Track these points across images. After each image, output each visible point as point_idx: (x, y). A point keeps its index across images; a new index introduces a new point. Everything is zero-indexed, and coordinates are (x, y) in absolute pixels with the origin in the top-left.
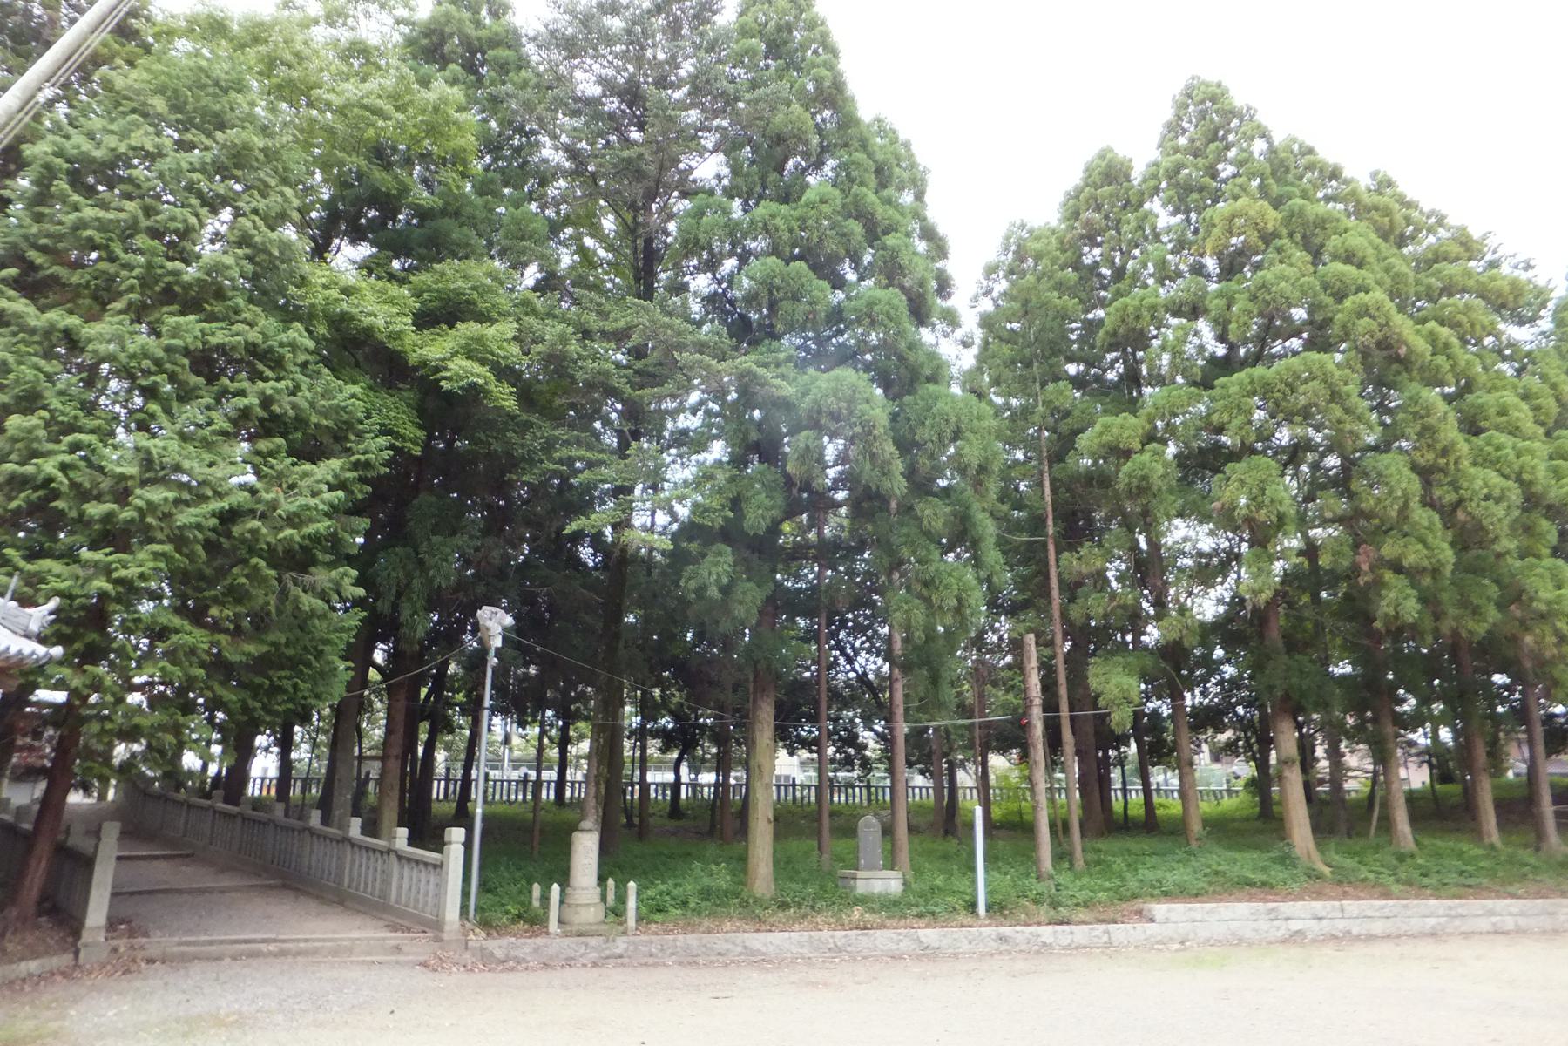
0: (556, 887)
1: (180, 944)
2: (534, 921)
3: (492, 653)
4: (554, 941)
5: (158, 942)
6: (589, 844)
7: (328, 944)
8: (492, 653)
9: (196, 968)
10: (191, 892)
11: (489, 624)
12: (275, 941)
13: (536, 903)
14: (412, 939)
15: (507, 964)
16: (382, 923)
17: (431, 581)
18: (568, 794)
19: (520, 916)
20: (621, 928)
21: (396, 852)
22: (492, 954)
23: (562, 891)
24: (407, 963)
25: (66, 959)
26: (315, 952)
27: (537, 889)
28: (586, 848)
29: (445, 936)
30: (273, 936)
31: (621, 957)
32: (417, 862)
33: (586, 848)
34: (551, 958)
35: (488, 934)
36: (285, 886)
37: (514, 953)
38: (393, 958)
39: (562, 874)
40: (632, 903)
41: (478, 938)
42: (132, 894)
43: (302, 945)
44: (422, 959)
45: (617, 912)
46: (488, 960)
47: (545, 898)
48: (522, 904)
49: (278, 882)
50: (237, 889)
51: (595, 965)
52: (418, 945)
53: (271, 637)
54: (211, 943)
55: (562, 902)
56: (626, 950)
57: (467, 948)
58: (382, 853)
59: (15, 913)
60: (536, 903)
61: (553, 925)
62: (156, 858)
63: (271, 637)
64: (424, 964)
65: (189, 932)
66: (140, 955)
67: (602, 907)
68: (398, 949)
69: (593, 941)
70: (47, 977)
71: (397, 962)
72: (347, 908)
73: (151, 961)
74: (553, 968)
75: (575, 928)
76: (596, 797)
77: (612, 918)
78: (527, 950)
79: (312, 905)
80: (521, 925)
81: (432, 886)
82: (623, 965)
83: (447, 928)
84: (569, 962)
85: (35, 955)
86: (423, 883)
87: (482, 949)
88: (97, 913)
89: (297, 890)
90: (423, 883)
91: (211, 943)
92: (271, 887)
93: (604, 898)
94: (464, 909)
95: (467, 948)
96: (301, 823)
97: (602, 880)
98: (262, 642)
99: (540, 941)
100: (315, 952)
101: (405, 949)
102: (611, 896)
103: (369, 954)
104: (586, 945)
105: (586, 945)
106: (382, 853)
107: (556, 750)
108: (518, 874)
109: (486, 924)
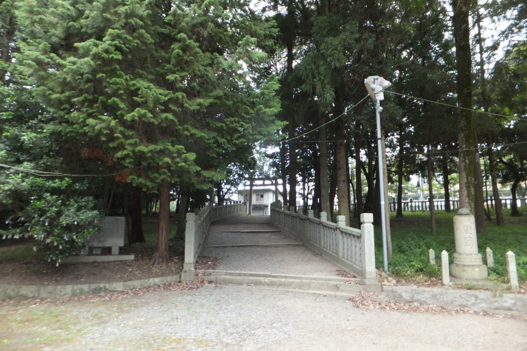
0: (445, 254)
1: (226, 274)
2: (433, 275)
3: (378, 104)
4: (446, 291)
5: (220, 272)
6: (468, 223)
7: (297, 281)
8: (378, 104)
9: (230, 288)
10: (262, 246)
11: (373, 86)
12: (270, 276)
13: (433, 262)
14: (346, 282)
15: (412, 306)
16: (335, 268)
17: (329, 65)
18: (452, 208)
19: (421, 270)
20: (505, 286)
21: (339, 229)
22: (401, 296)
23: (450, 256)
24: (341, 297)
25: (176, 278)
26: (289, 285)
27: (432, 253)
28: (466, 228)
29: (367, 282)
30: (269, 273)
31: (510, 309)
32: (350, 234)
33: (466, 228)
34: (447, 303)
35: (398, 282)
36: (303, 245)
37: (417, 297)
38: (333, 293)
39: (450, 244)
40: (512, 267)
41: (390, 283)
42: (239, 246)
43: (283, 280)
44: (351, 295)
45: (499, 271)
46: (397, 302)
47: (438, 258)
48: (422, 261)
49: (301, 243)
50: (283, 246)
51: (486, 313)
52: (350, 288)
53: (215, 93)
54: (240, 275)
55: (451, 262)
56: (515, 304)
57: (382, 290)
58: (334, 229)
59: (158, 254)
60: (433, 262)
61: (446, 278)
62: (268, 232)
63: (215, 93)
64: (351, 299)
65: (236, 268)
66: (207, 278)
67: (484, 268)
68: (337, 287)
69: (482, 294)
70: (167, 286)
71: (335, 296)
72: (323, 258)
73: (210, 282)
74: (449, 312)
75: (464, 282)
76: (469, 195)
77: (494, 276)
78: (427, 295)
79: (309, 255)
80: (421, 277)
81: (358, 249)
82: (512, 317)
83: (368, 276)
84: (462, 309)
85: (157, 276)
86: (354, 247)
87: (393, 292)
88: (190, 256)
89: (307, 247)
90: (354, 247)
91: (240, 275)
92: (298, 246)
93: (485, 262)
94: (379, 264)
95: (382, 290)
96: (305, 216)
97: (481, 248)
98: (210, 97)
99: (436, 290)
100: (289, 285)
101: (341, 287)
102: (491, 260)
103: (319, 288)
104: (476, 297)
105: (476, 297)
106: (334, 229)
107: (443, 189)
108: (421, 243)
109: (397, 274)
